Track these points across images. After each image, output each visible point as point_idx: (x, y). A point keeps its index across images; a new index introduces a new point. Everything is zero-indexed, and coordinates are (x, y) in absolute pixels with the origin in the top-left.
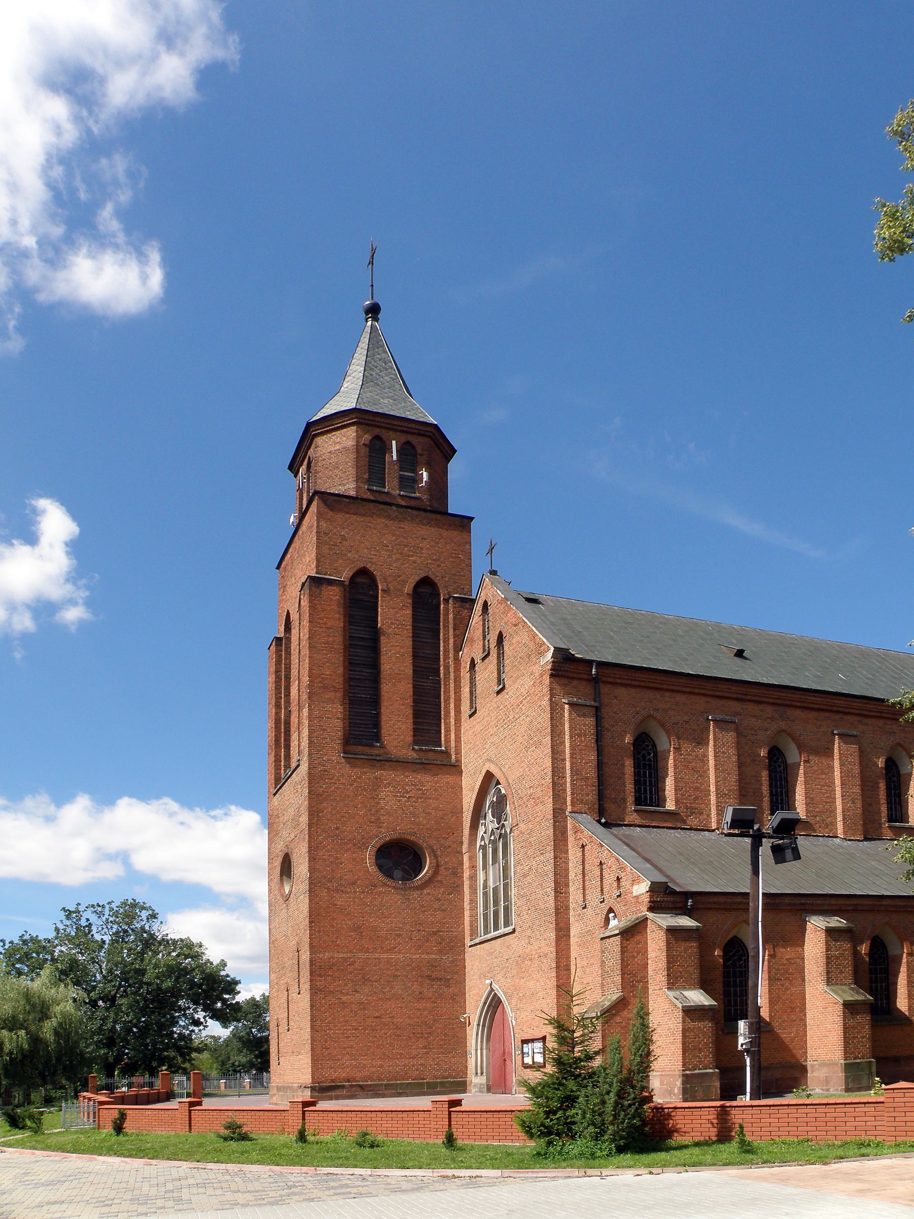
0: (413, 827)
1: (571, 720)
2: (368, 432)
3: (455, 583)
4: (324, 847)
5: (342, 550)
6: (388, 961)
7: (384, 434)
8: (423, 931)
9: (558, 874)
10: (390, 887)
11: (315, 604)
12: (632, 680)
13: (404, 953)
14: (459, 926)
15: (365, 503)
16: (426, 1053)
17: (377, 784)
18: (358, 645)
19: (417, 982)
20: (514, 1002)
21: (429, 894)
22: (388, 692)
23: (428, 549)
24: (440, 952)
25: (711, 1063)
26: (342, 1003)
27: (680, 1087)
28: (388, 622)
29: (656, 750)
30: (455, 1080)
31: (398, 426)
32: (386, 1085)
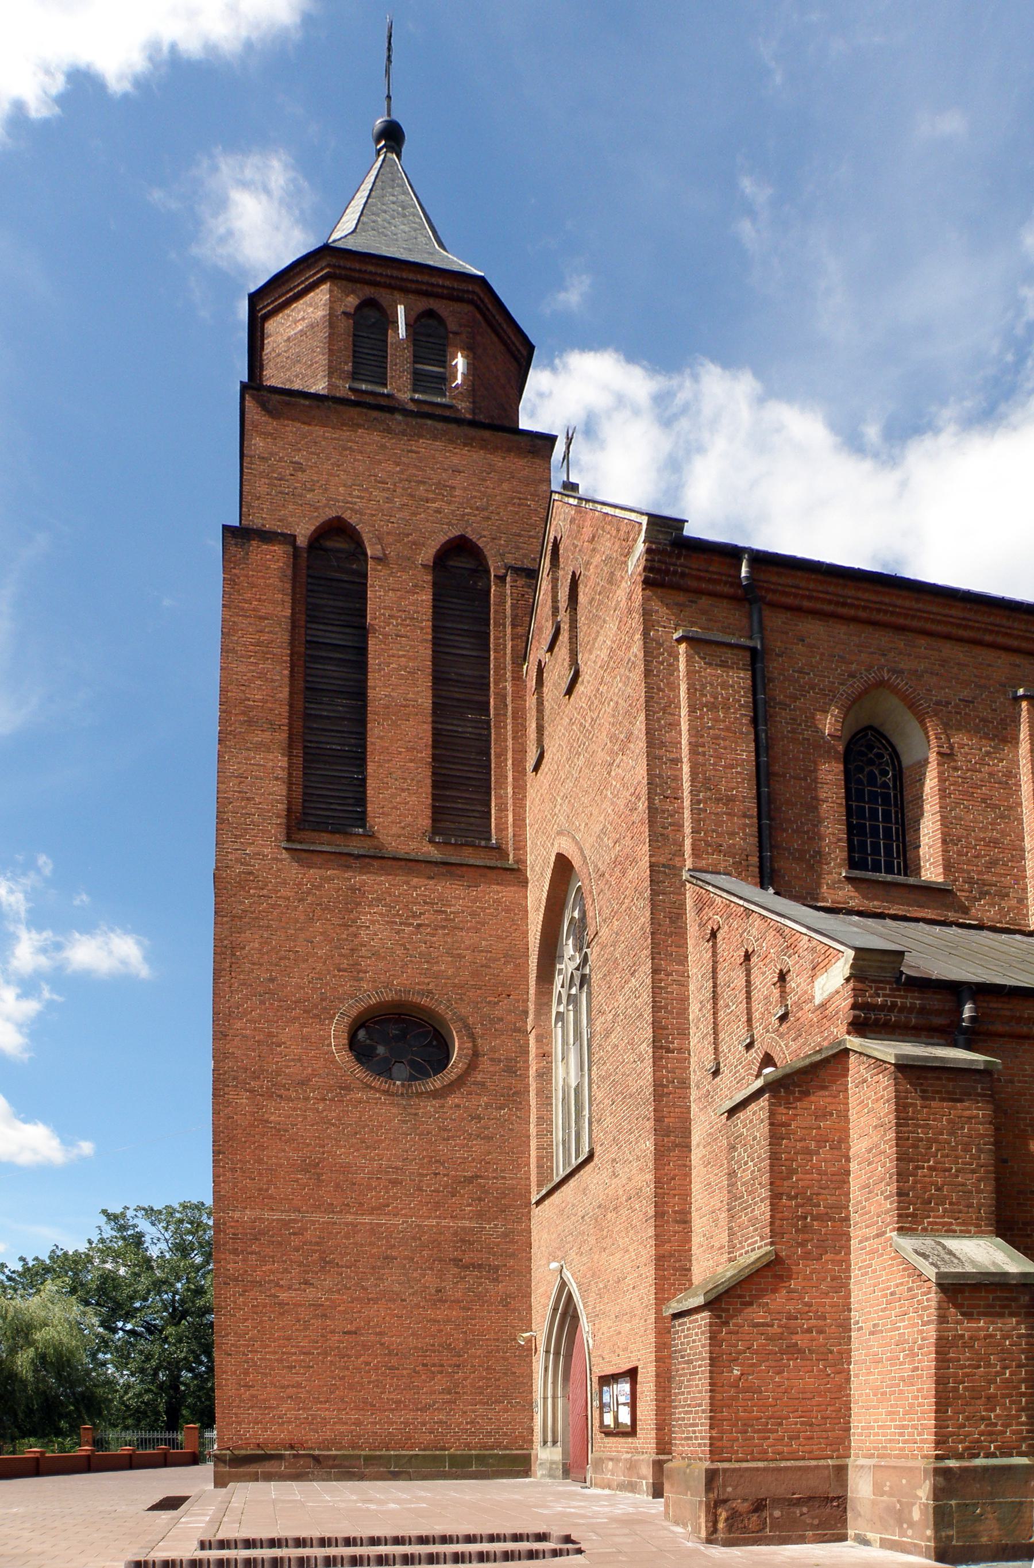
0: (427, 980)
1: (690, 673)
2: (353, 292)
3: (518, 548)
4: (245, 1013)
5: (296, 488)
6: (373, 1230)
7: (383, 296)
8: (444, 1175)
9: (661, 1008)
10: (377, 1090)
11: (236, 575)
12: (837, 603)
13: (405, 1215)
14: (519, 1167)
15: (340, 408)
16: (449, 1402)
17: (354, 899)
18: (331, 658)
19: (432, 1269)
20: (592, 1298)
21: (458, 1106)
22: (381, 738)
23: (465, 489)
24: (480, 1215)
25: (1024, 1439)
26: (279, 1304)
27: (926, 1505)
28: (384, 615)
29: (900, 762)
30: (508, 1452)
31: (412, 281)
32: (368, 1459)
